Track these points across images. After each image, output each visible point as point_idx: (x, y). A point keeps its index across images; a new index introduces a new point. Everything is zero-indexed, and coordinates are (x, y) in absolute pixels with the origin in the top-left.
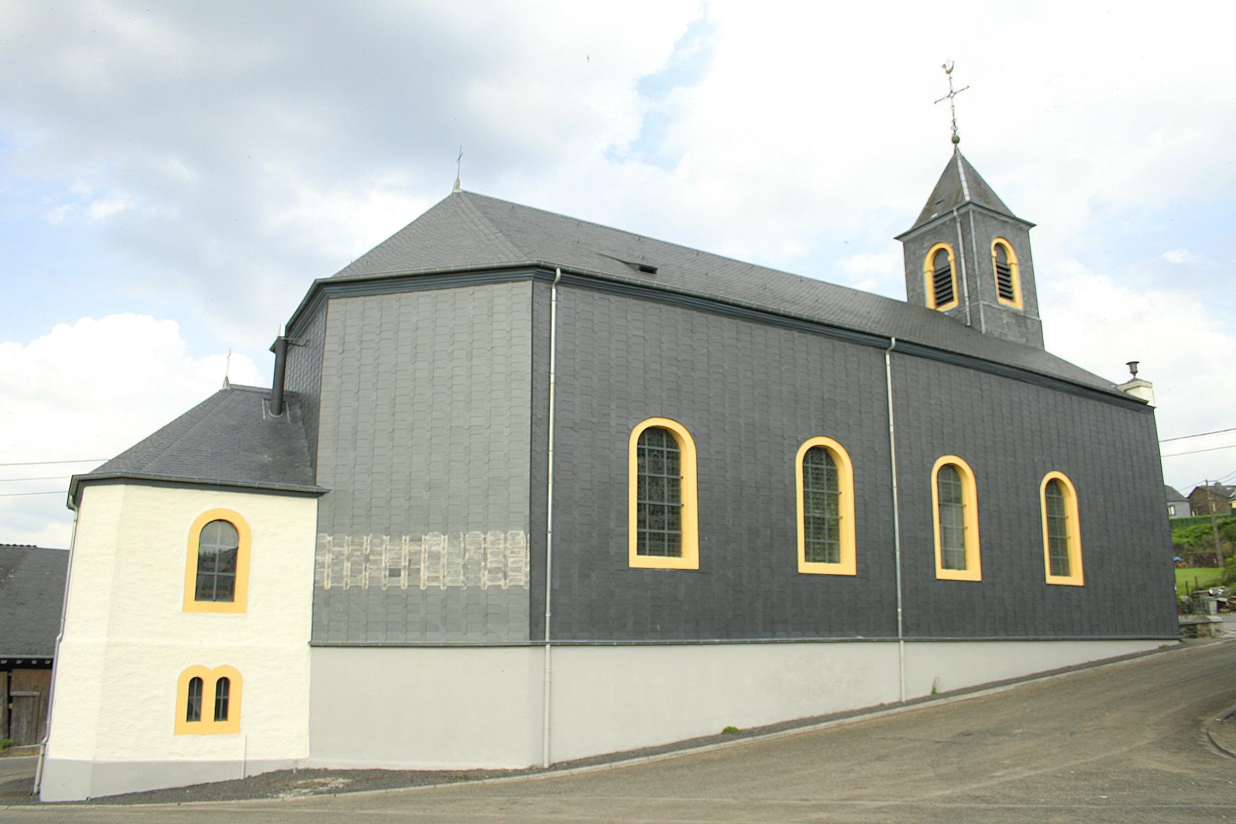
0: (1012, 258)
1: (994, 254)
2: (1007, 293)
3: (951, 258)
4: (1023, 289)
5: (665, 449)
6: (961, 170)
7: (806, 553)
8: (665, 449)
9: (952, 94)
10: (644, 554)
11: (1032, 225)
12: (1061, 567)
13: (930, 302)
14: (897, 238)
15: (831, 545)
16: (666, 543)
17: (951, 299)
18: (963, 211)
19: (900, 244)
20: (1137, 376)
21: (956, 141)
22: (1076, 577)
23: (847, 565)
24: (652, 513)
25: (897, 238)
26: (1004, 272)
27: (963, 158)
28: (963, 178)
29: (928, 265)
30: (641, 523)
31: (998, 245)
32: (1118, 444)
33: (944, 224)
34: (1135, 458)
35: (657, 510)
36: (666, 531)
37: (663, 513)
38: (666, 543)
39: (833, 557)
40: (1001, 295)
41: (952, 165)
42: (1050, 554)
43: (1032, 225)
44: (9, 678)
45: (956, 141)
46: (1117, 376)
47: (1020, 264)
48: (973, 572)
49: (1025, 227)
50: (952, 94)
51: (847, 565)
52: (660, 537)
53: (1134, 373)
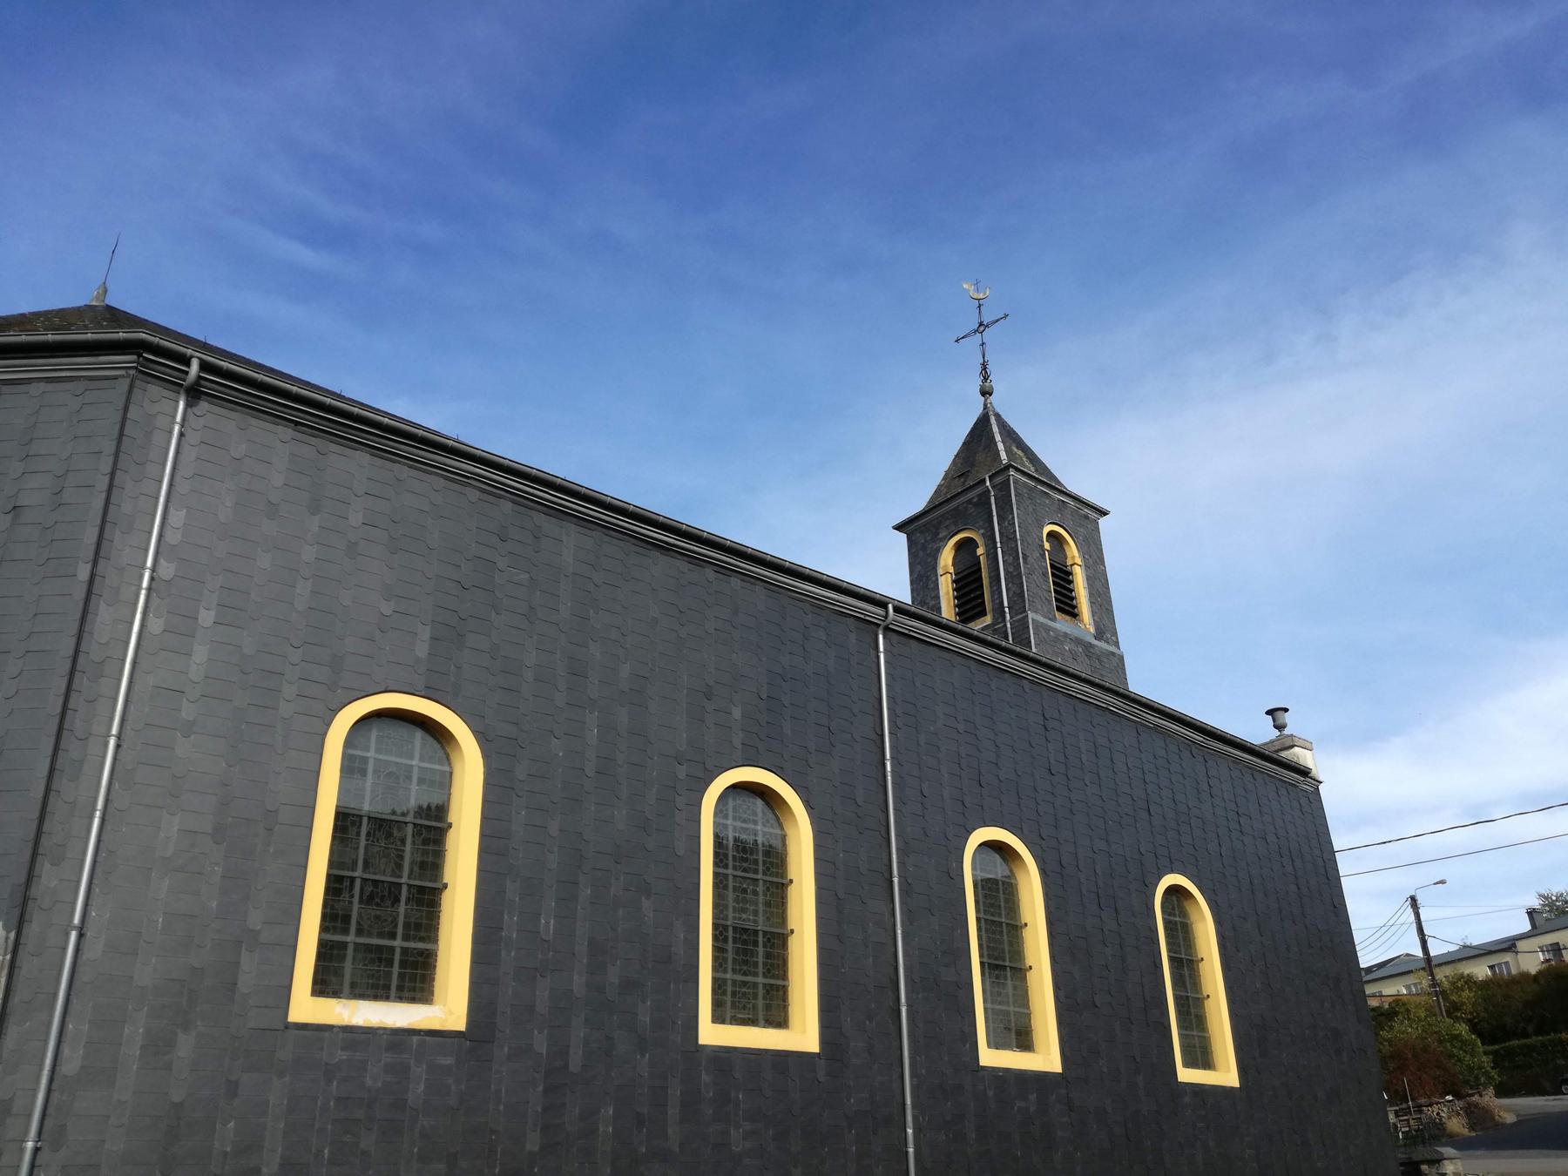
0: (1073, 552)
1: (1047, 546)
2: (1067, 606)
3: (980, 551)
4: (1092, 603)
5: (760, 980)
6: (995, 429)
7: (717, 1005)
8: (760, 980)
9: (982, 326)
10: (723, 1022)
11: (1104, 513)
12: (1201, 1056)
13: (948, 611)
14: (899, 528)
15: (769, 989)
16: (396, 970)
17: (983, 613)
18: (999, 479)
19: (903, 537)
20: (1287, 731)
21: (986, 393)
22: (1046, 1057)
23: (802, 1033)
24: (367, 900)
25: (899, 528)
26: (1063, 577)
27: (998, 416)
28: (998, 438)
29: (946, 558)
30: (332, 918)
31: (1051, 535)
32: (1271, 838)
33: (970, 502)
34: (1298, 863)
35: (381, 894)
36: (398, 943)
37: (397, 900)
38: (396, 970)
39: (777, 1017)
40: (1059, 609)
41: (980, 434)
42: (1179, 1027)
43: (1104, 513)
44: (1440, 965)
45: (986, 393)
46: (1258, 732)
47: (1087, 567)
48: (1046, 1057)
49: (1092, 515)
50: (982, 326)
51: (802, 1033)
52: (381, 956)
53: (1280, 727)
